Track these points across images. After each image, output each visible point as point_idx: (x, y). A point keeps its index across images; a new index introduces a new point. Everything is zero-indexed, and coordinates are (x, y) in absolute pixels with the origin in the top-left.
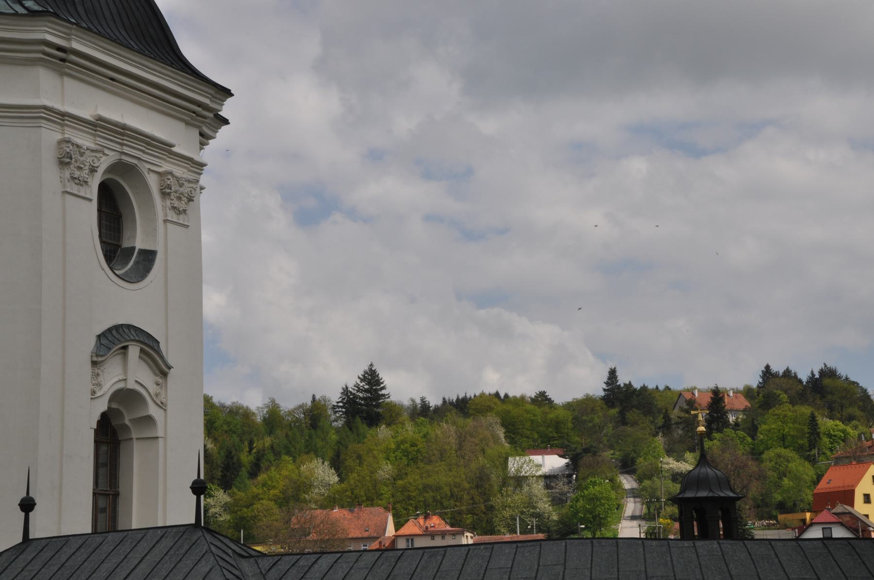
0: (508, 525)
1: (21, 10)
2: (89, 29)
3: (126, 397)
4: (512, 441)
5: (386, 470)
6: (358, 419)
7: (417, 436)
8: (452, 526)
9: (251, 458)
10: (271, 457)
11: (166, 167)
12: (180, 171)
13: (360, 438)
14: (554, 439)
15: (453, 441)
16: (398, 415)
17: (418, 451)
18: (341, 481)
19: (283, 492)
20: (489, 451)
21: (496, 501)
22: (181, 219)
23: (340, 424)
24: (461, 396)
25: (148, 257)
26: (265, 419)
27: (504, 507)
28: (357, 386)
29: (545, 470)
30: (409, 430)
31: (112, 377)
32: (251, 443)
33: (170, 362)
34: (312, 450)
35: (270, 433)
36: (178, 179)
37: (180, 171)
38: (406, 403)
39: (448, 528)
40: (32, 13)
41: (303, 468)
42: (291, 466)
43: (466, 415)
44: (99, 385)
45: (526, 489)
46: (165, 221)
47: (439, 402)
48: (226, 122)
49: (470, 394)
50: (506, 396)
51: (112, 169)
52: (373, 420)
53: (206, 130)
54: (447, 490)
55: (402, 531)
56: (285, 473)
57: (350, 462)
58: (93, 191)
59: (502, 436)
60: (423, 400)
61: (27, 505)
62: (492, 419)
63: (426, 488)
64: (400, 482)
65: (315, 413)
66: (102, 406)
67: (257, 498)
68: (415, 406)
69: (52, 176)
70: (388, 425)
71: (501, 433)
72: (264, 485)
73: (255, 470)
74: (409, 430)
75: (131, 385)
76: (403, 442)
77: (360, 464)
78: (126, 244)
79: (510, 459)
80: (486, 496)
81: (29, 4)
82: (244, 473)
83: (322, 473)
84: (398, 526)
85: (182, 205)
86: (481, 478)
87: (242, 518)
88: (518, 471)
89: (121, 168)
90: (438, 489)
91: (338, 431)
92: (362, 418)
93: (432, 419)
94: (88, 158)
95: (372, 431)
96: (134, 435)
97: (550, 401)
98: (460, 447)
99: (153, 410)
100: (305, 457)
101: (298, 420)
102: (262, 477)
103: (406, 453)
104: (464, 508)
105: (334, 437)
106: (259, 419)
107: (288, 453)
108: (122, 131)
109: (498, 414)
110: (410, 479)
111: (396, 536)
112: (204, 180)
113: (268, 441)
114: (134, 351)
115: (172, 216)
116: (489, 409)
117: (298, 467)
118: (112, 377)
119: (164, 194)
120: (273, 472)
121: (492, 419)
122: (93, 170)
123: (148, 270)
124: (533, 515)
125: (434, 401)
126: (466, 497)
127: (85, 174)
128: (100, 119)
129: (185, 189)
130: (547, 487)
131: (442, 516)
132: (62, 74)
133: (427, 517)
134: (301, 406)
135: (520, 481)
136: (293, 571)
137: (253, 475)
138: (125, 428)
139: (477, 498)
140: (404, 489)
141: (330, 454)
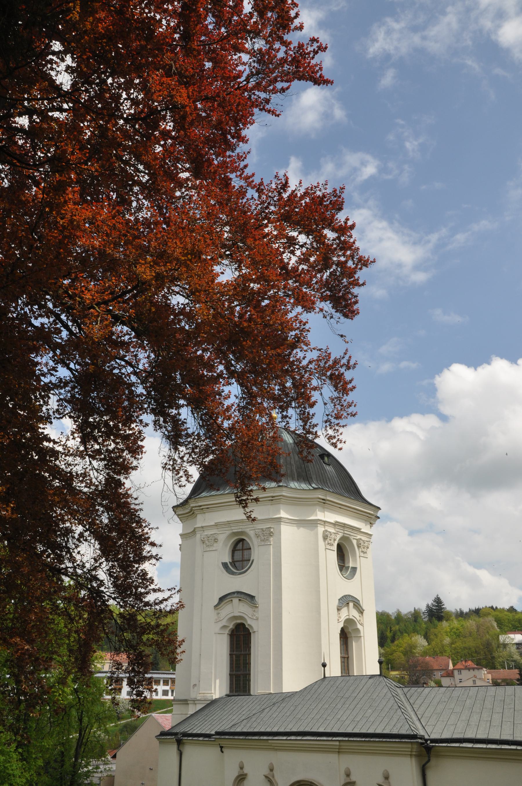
0: (501, 665)
1: (312, 488)
2: (333, 492)
3: (349, 622)
4: (500, 628)
5: (447, 640)
6: (434, 618)
7: (459, 626)
8: (477, 665)
9: (391, 634)
10: (399, 634)
11: (359, 537)
12: (364, 538)
13: (435, 627)
14: (518, 627)
15: (474, 627)
16: (451, 616)
17: (460, 632)
18: (429, 644)
19: (405, 649)
20: (490, 632)
21: (496, 654)
22: (365, 555)
23: (426, 619)
24: (477, 608)
25: (354, 569)
26: (395, 618)
27: (499, 657)
28: (432, 604)
29: (516, 641)
30: (456, 624)
31: (344, 614)
32: (391, 628)
33: (364, 608)
34: (415, 631)
35: (398, 624)
36: (363, 541)
37: (364, 538)
38: (454, 611)
39: (476, 666)
40: (315, 489)
41: (413, 639)
42: (408, 638)
43: (480, 617)
44: (340, 617)
45: (508, 649)
46: (360, 556)
47: (468, 610)
48: (379, 518)
49: (481, 607)
50: (496, 608)
51: (341, 539)
52: (440, 618)
53: (372, 522)
54: (473, 649)
55: (456, 667)
56: (405, 641)
57: (432, 637)
58: (335, 548)
59: (496, 626)
60: (460, 609)
61: (324, 665)
62: (490, 618)
63: (465, 648)
64: (453, 646)
65: (416, 615)
66: (341, 625)
67: (395, 651)
68: (457, 612)
69: (321, 543)
70: (447, 621)
71: (495, 624)
72: (397, 646)
73: (393, 640)
74: (456, 624)
75: (351, 617)
76: (453, 628)
77: (437, 638)
78: (347, 565)
79: (500, 636)
80: (491, 652)
81: (314, 485)
82: (389, 641)
83: (420, 641)
84: (454, 665)
85: (365, 550)
86: (488, 644)
87: (389, 660)
88: (504, 641)
89: (345, 538)
90: (470, 649)
91: (426, 623)
92: (436, 618)
93: (465, 618)
94: (333, 536)
95: (440, 623)
96: (353, 635)
97: (516, 611)
98: (478, 631)
99: (359, 626)
100: (413, 634)
101: (409, 618)
102: (396, 642)
103: (455, 633)
104: (481, 657)
105: (424, 626)
106: (393, 618)
107: (406, 632)
108: (344, 526)
109: (493, 616)
110: (457, 644)
111: (453, 669)
112: (371, 540)
113: (397, 627)
114: (351, 605)
115: (362, 554)
116: (489, 614)
117: (411, 639)
118: (344, 614)
119: (359, 547)
120: (400, 640)
121: (490, 618)
122: (335, 540)
123: (354, 574)
124: (512, 661)
125: (466, 610)
126: (482, 652)
127: (332, 542)
128: (337, 522)
129: (366, 544)
130: (518, 648)
131: (472, 661)
132: (324, 508)
133: (466, 661)
134: (410, 612)
135: (505, 645)
136: (416, 693)
137: (393, 641)
138: (350, 633)
139: (487, 653)
140: (455, 649)
141: (423, 633)
